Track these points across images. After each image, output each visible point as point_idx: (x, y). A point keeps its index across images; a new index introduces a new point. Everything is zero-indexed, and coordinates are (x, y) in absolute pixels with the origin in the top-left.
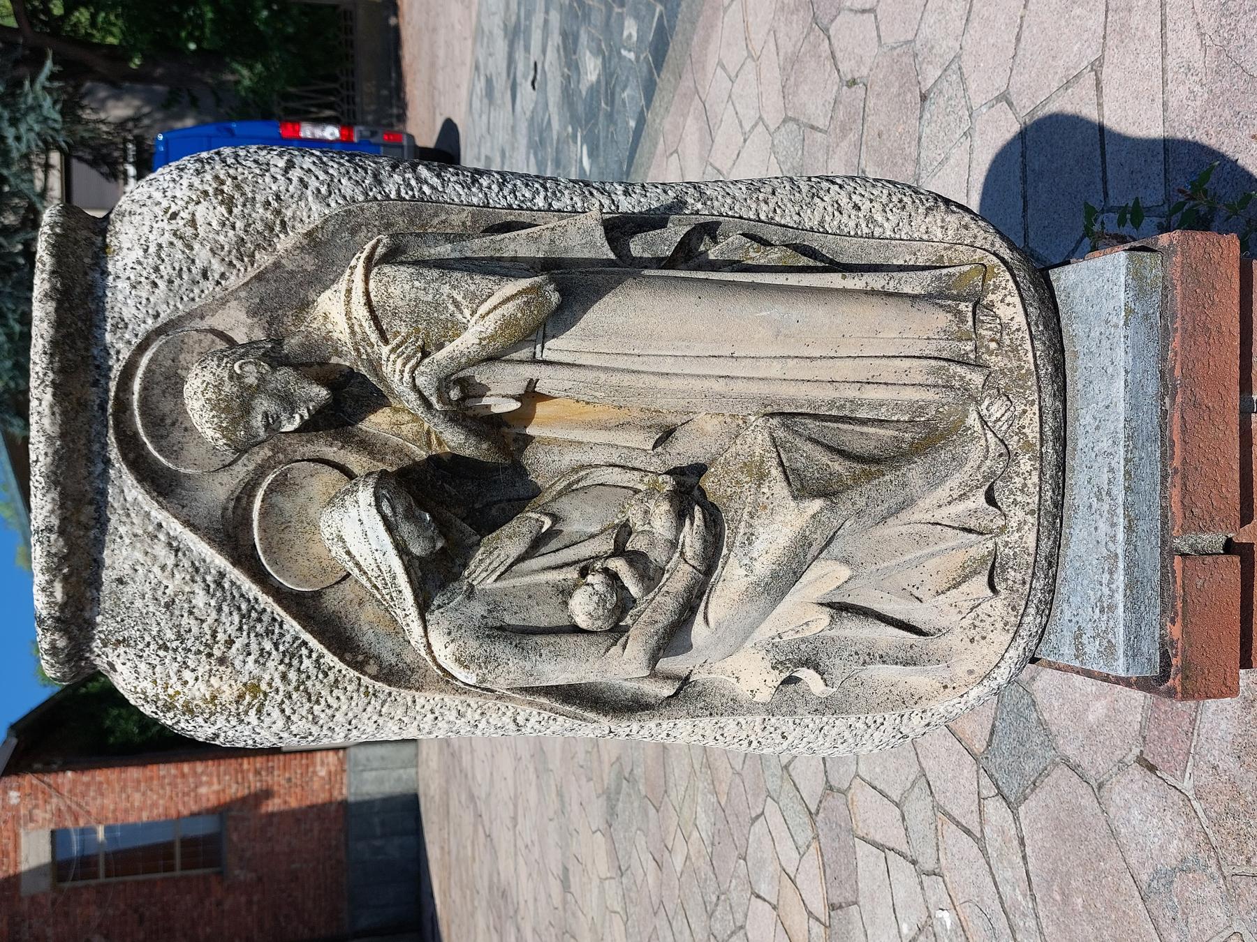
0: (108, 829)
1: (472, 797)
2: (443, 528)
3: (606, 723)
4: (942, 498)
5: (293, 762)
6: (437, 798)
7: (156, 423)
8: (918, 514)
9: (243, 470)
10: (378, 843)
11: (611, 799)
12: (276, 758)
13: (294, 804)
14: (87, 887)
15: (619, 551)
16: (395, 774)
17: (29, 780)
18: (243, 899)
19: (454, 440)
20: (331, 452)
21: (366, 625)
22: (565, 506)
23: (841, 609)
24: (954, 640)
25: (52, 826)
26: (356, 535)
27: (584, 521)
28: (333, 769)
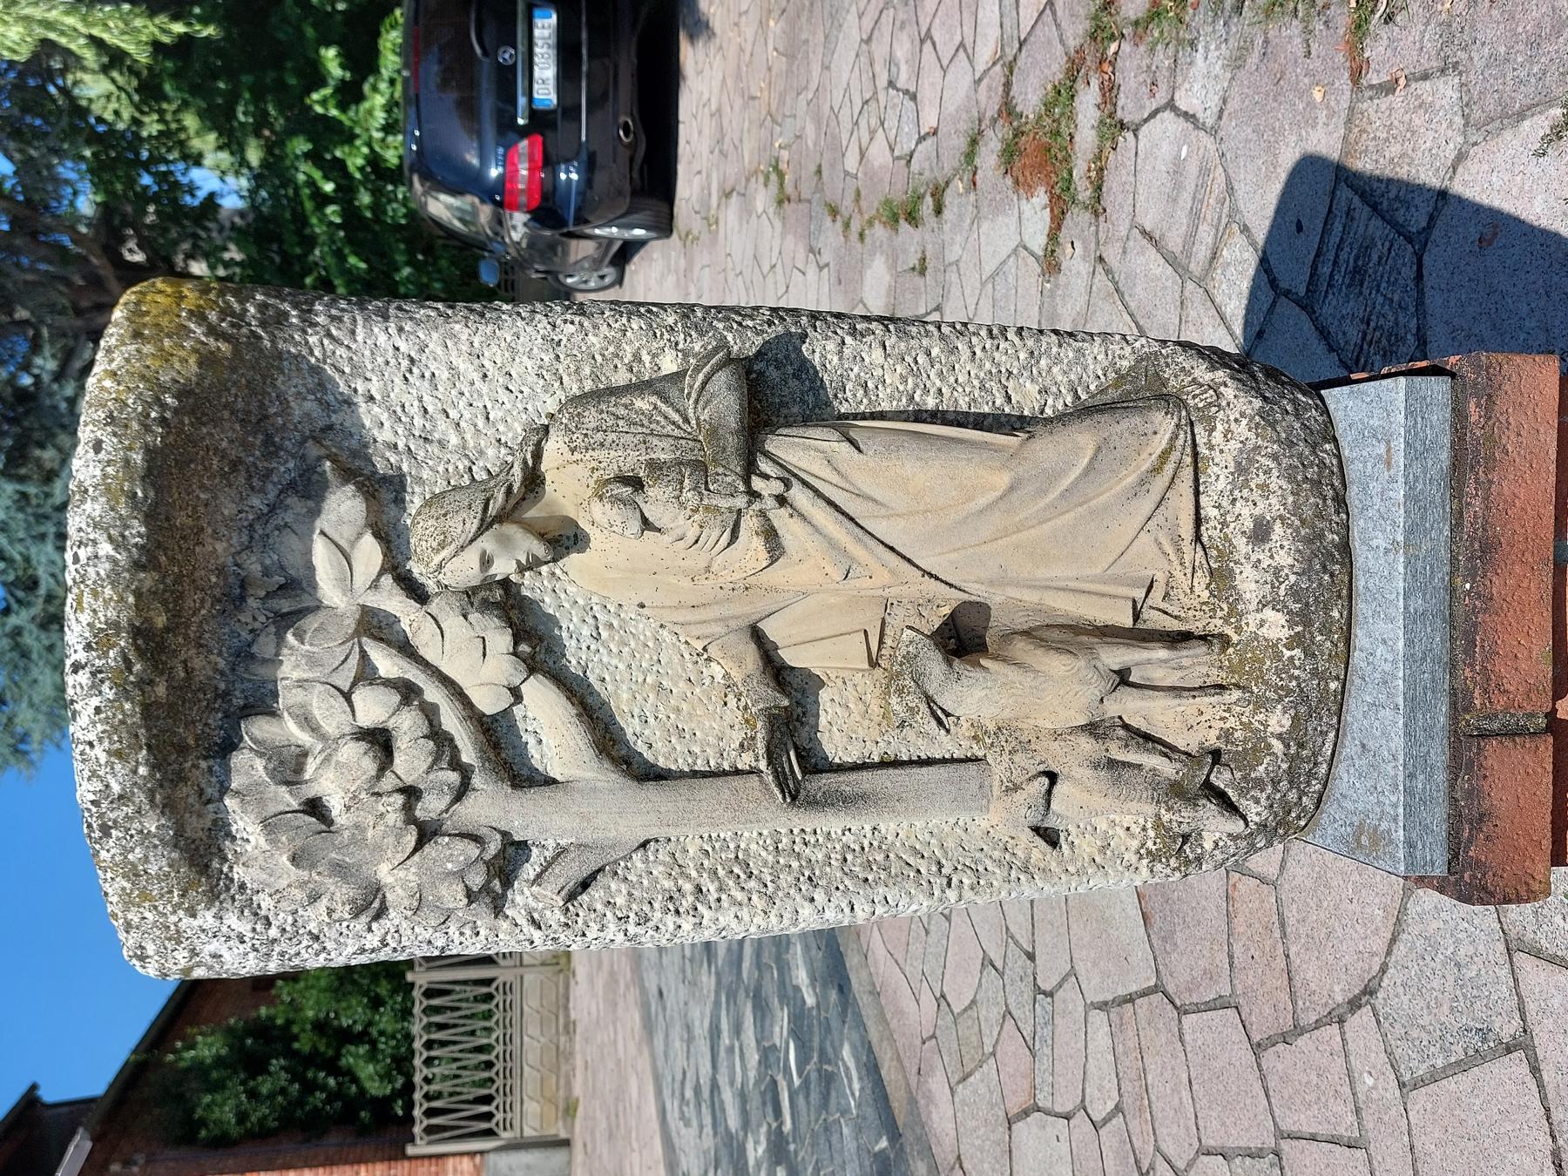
5: (421, 1170)
12: (399, 1164)
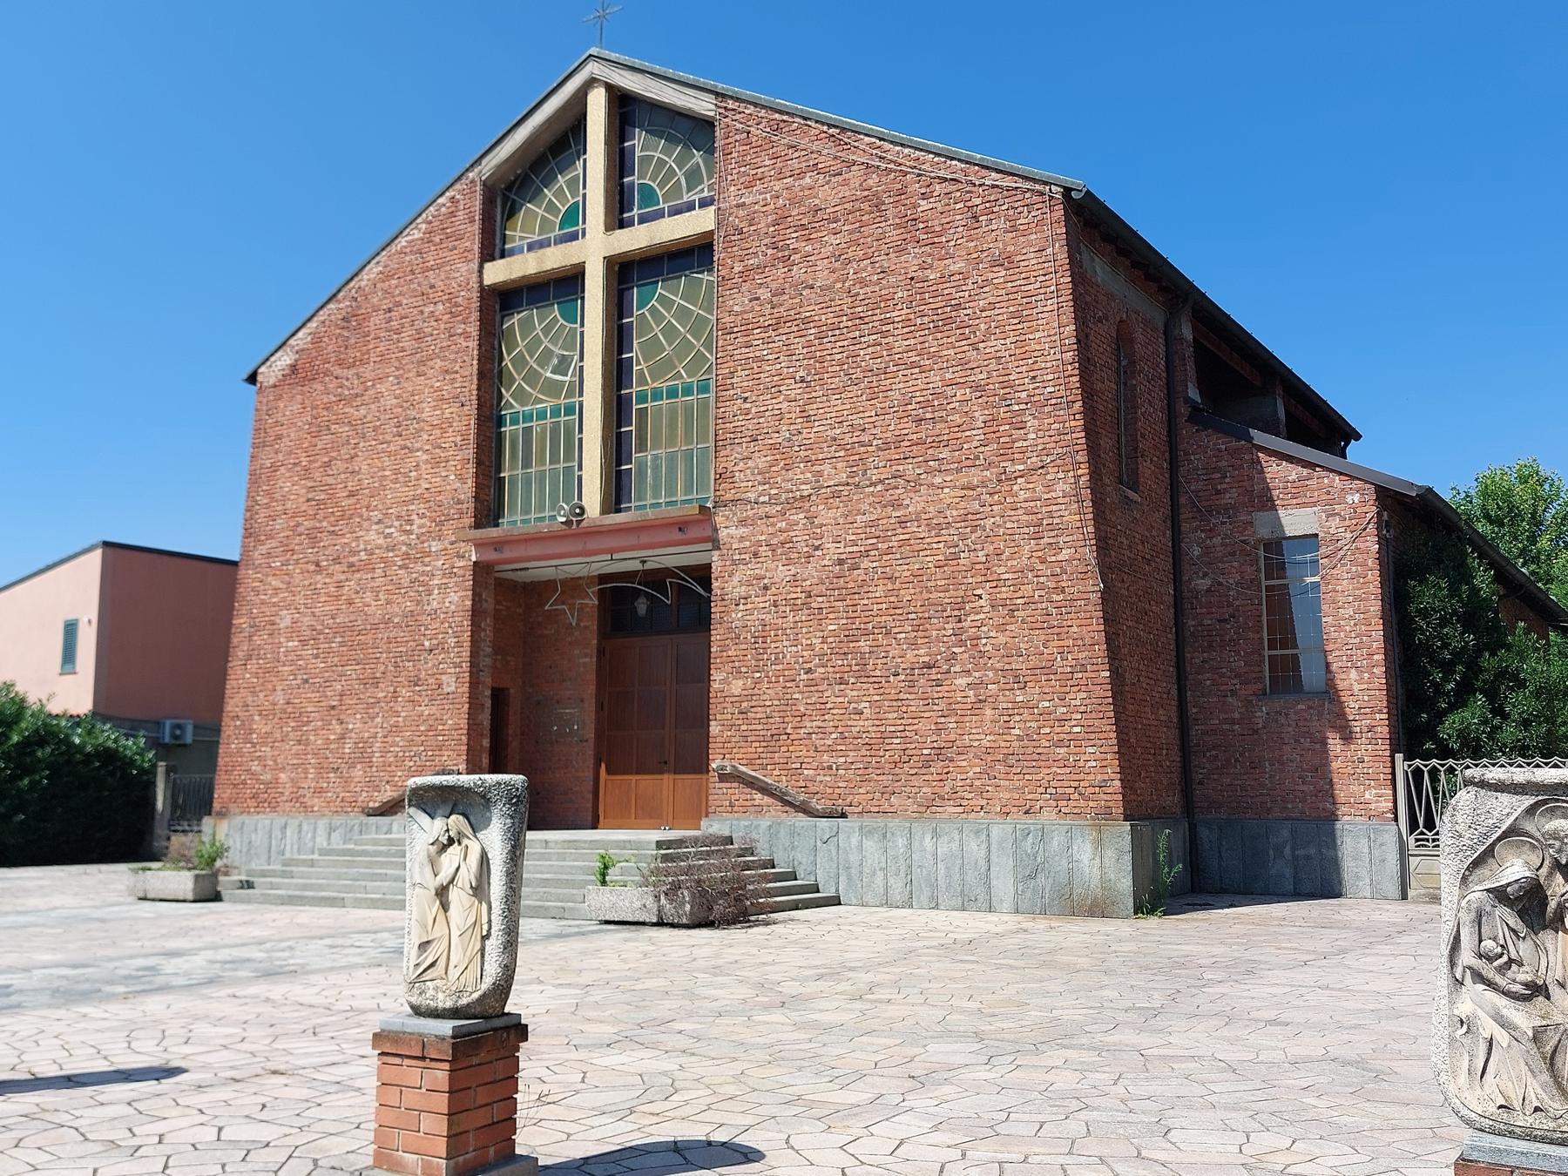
1: (1343, 951)
3: (1446, 953)
4: (1537, 1089)
6: (1337, 917)
7: (1552, 810)
8: (1530, 1079)
9: (1538, 834)
10: (1287, 851)
11: (1360, 1063)
14: (1258, 570)
15: (1511, 961)
16: (1364, 873)
17: (1372, 510)
18: (1237, 715)
19: (1553, 904)
20: (1547, 862)
21: (1482, 872)
22: (1529, 942)
24: (1479, 1092)
25: (1321, 535)
26: (1514, 869)
27: (1524, 949)
28: (1373, 806)
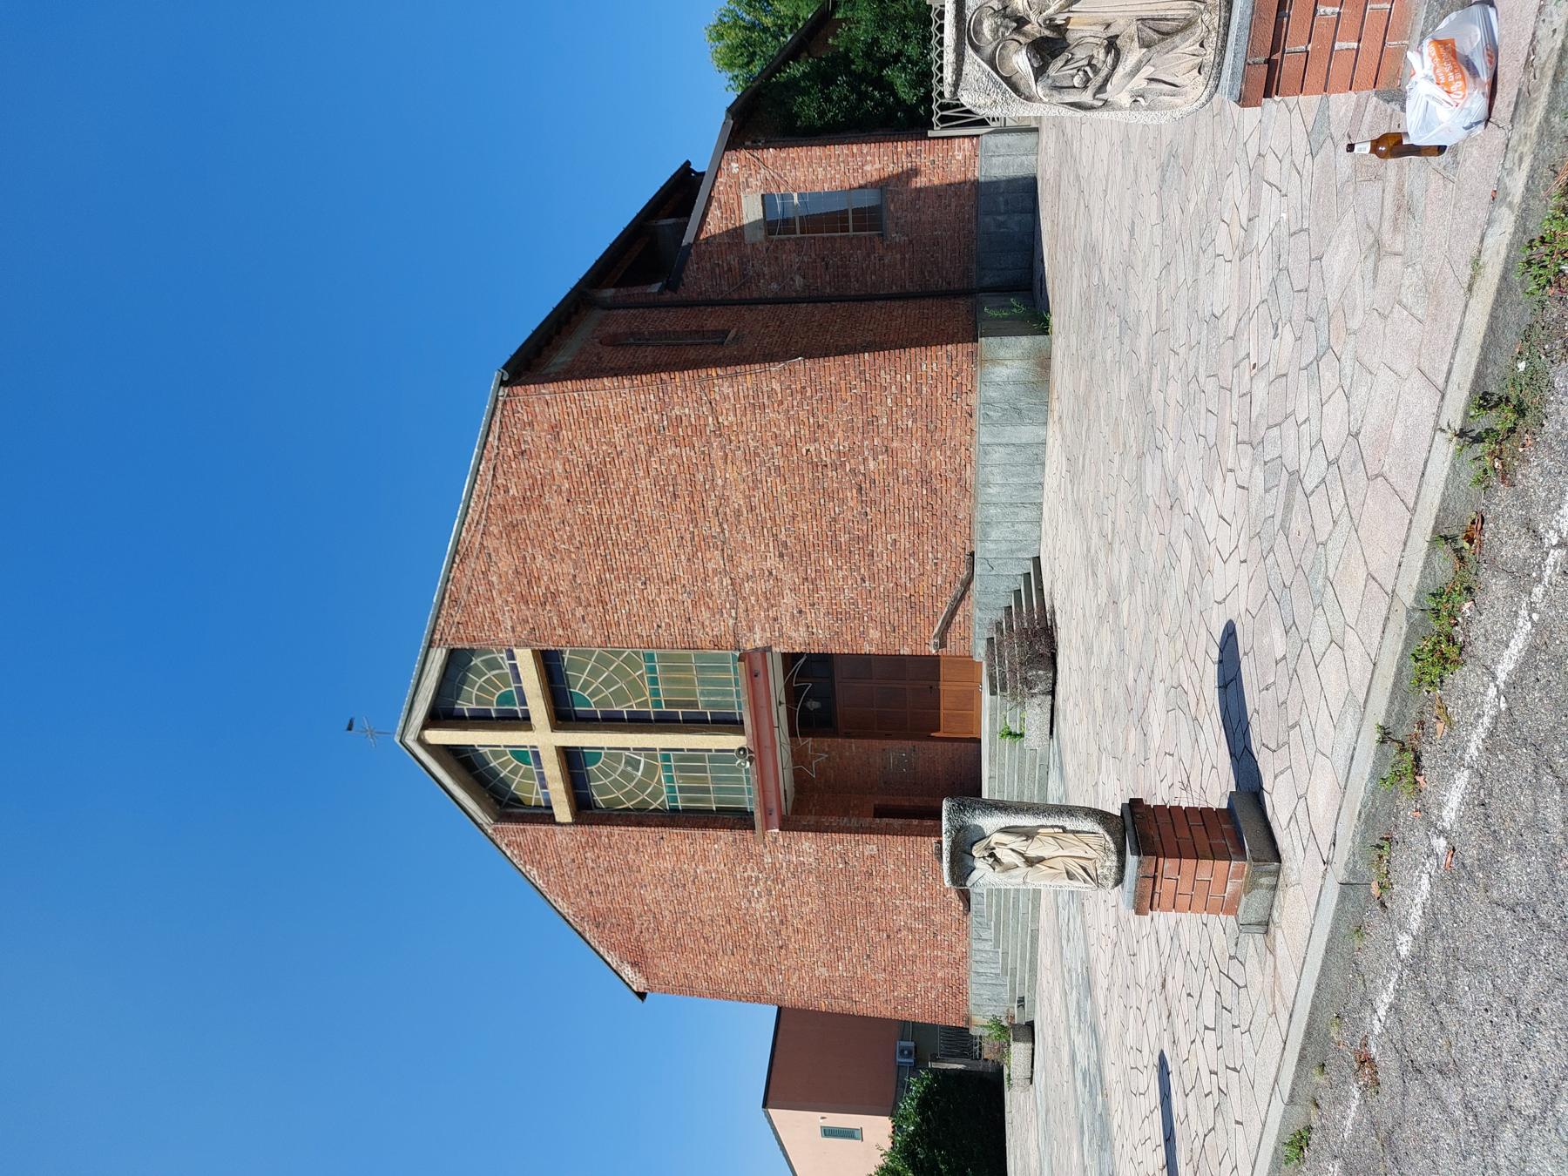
0: (801, 196)
1: (1078, 177)
2: (1042, 58)
4: (1186, 46)
10: (1001, 218)
11: (1164, 169)
13: (936, 182)
19: (1047, 33)
22: (1075, 50)
23: (1151, 80)
26: (1021, 62)
27: (1081, 54)
